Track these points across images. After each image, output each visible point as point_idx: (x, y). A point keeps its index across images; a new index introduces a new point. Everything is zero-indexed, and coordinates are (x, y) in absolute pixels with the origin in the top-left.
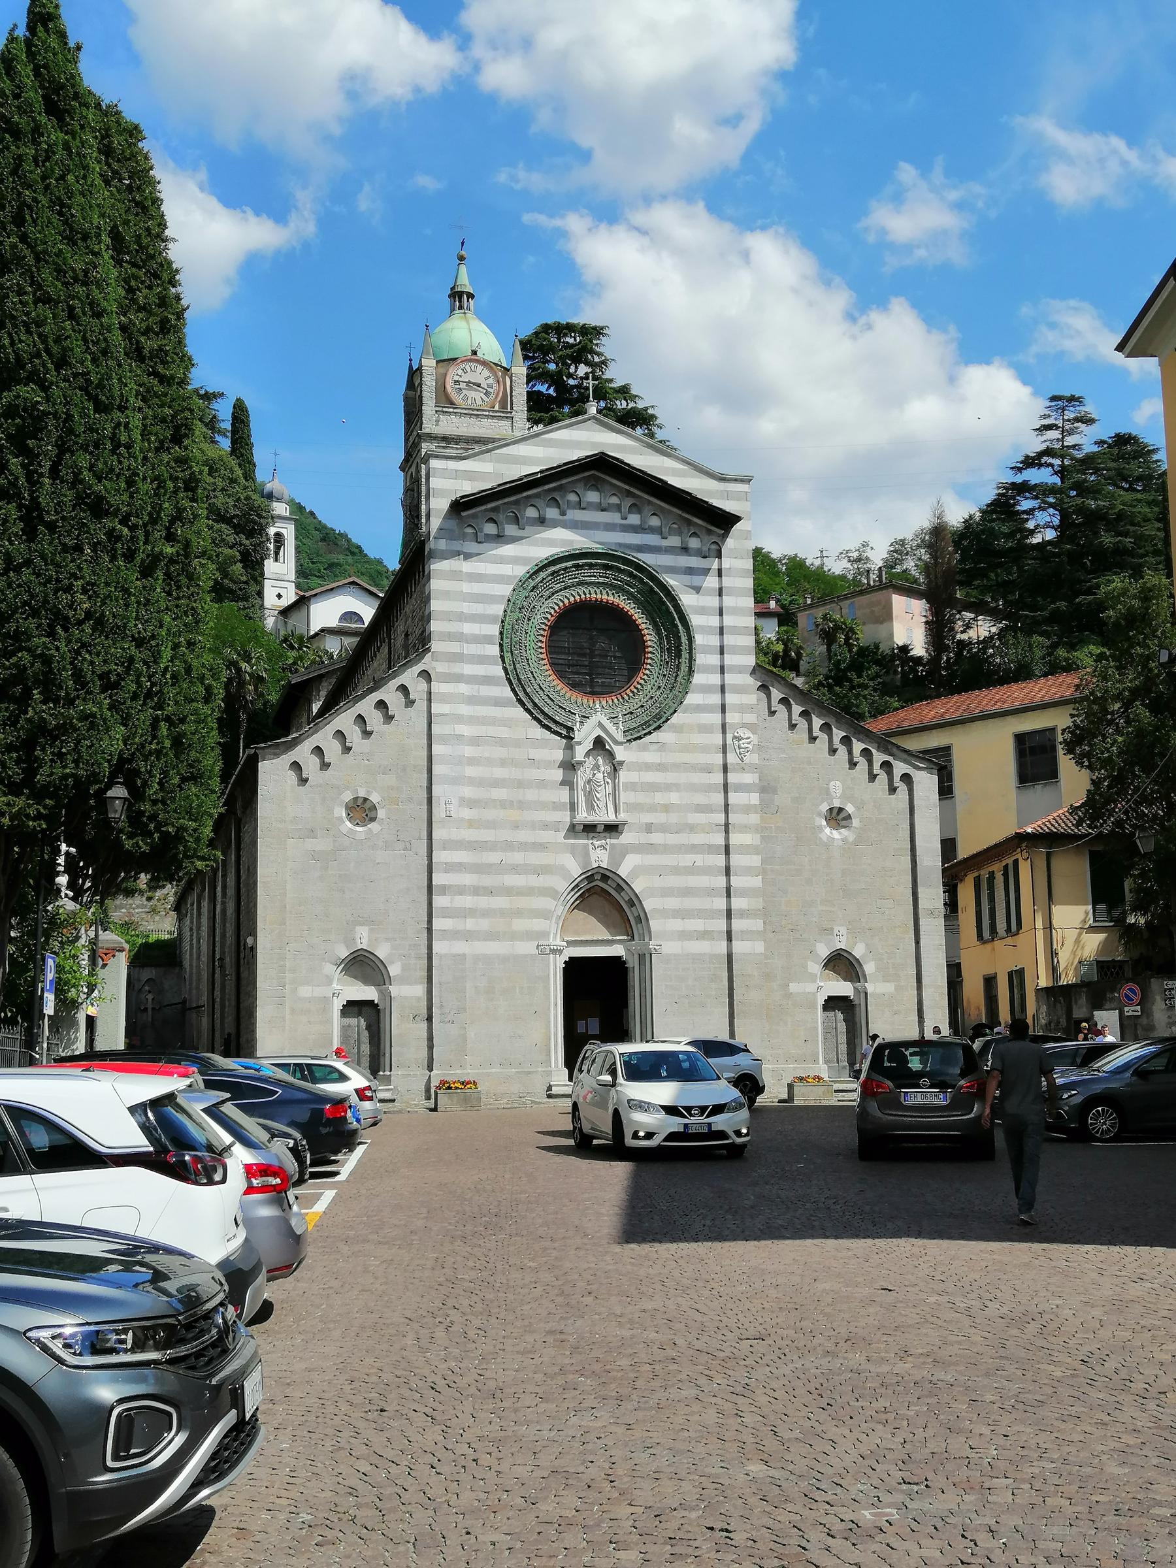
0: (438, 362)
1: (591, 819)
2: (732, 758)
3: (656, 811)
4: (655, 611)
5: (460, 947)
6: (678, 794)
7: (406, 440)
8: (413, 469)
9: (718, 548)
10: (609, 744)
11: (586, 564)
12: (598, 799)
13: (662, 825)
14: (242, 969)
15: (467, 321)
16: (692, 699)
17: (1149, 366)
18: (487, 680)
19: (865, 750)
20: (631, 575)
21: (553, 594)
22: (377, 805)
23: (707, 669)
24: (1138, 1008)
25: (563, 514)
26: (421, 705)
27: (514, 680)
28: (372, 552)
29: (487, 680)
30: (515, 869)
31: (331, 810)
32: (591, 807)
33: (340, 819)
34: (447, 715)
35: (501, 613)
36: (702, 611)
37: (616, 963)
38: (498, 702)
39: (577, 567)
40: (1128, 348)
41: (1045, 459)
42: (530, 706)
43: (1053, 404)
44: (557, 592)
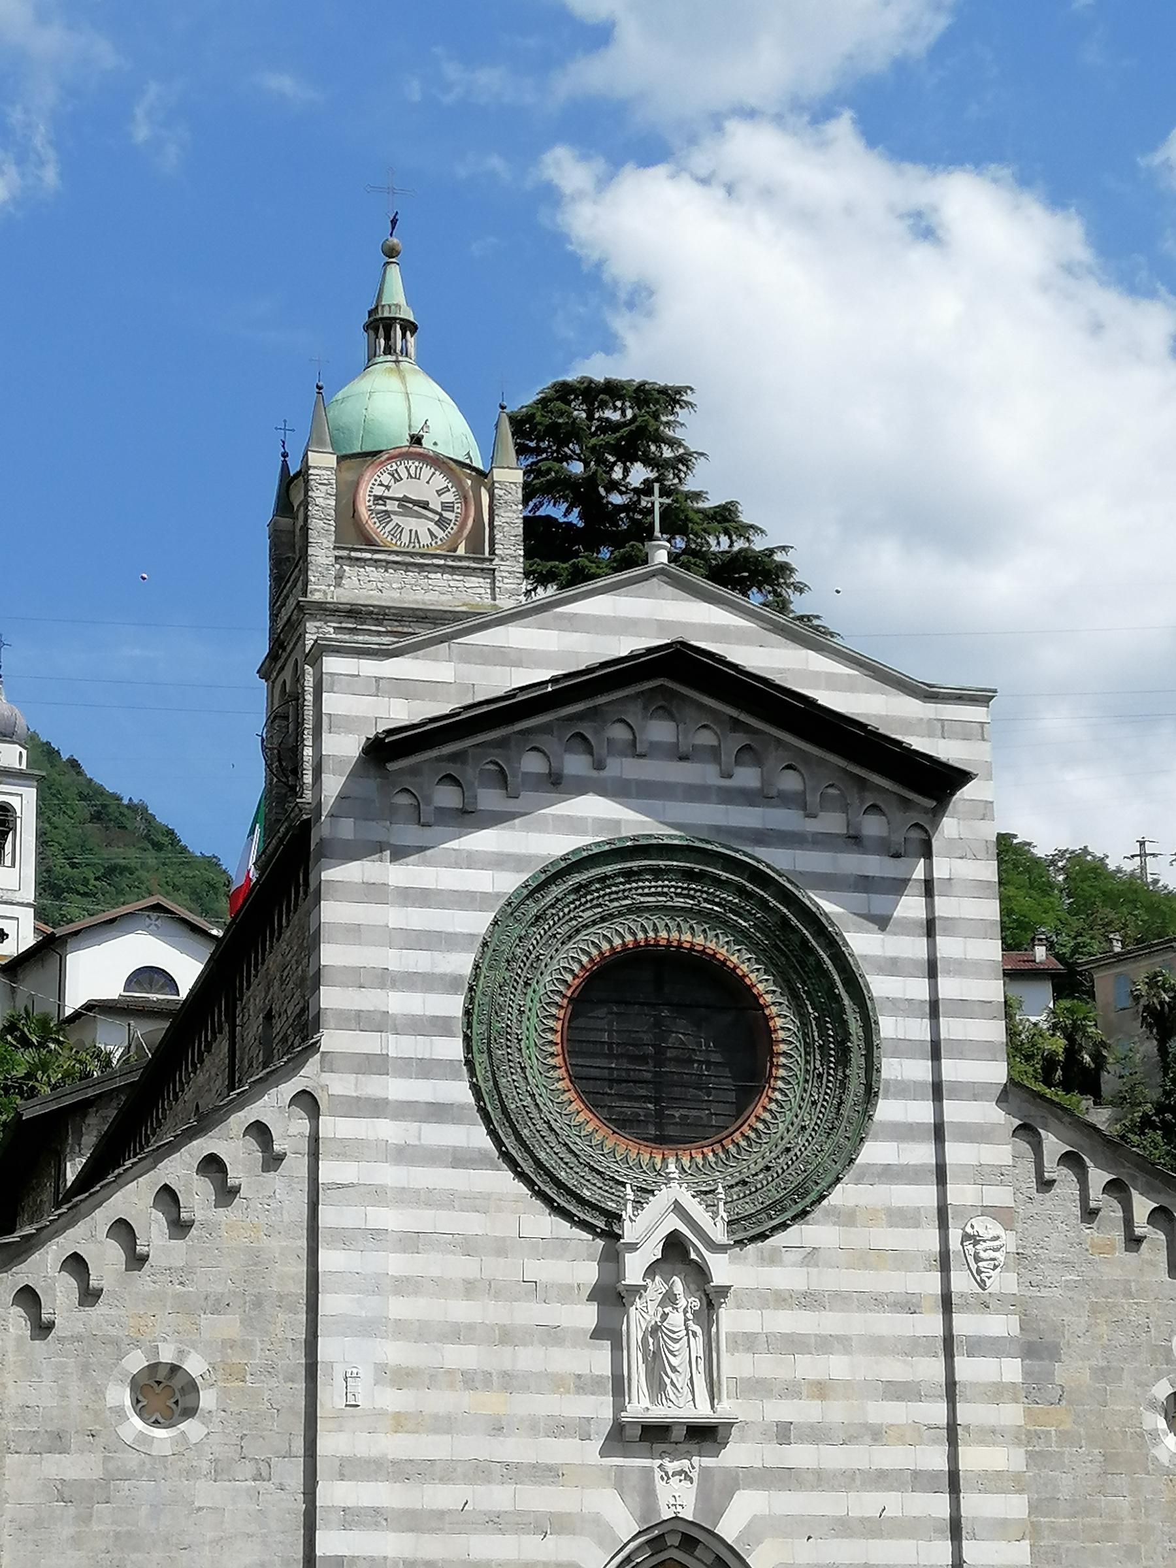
1: (660, 1412)
2: (961, 1282)
6: (846, 1358)
7: (274, 617)
8: (287, 674)
9: (924, 836)
12: (674, 1369)
13: (812, 1426)
15: (403, 379)
16: (873, 1152)
18: (438, 1112)
20: (741, 891)
22: (199, 1381)
23: (905, 1090)
25: (599, 766)
26: (296, 1165)
29: (438, 1112)
30: (496, 1522)
31: (99, 1392)
32: (657, 1387)
33: (119, 1412)
35: (468, 970)
36: (893, 966)
38: (460, 1159)
42: (528, 1167)
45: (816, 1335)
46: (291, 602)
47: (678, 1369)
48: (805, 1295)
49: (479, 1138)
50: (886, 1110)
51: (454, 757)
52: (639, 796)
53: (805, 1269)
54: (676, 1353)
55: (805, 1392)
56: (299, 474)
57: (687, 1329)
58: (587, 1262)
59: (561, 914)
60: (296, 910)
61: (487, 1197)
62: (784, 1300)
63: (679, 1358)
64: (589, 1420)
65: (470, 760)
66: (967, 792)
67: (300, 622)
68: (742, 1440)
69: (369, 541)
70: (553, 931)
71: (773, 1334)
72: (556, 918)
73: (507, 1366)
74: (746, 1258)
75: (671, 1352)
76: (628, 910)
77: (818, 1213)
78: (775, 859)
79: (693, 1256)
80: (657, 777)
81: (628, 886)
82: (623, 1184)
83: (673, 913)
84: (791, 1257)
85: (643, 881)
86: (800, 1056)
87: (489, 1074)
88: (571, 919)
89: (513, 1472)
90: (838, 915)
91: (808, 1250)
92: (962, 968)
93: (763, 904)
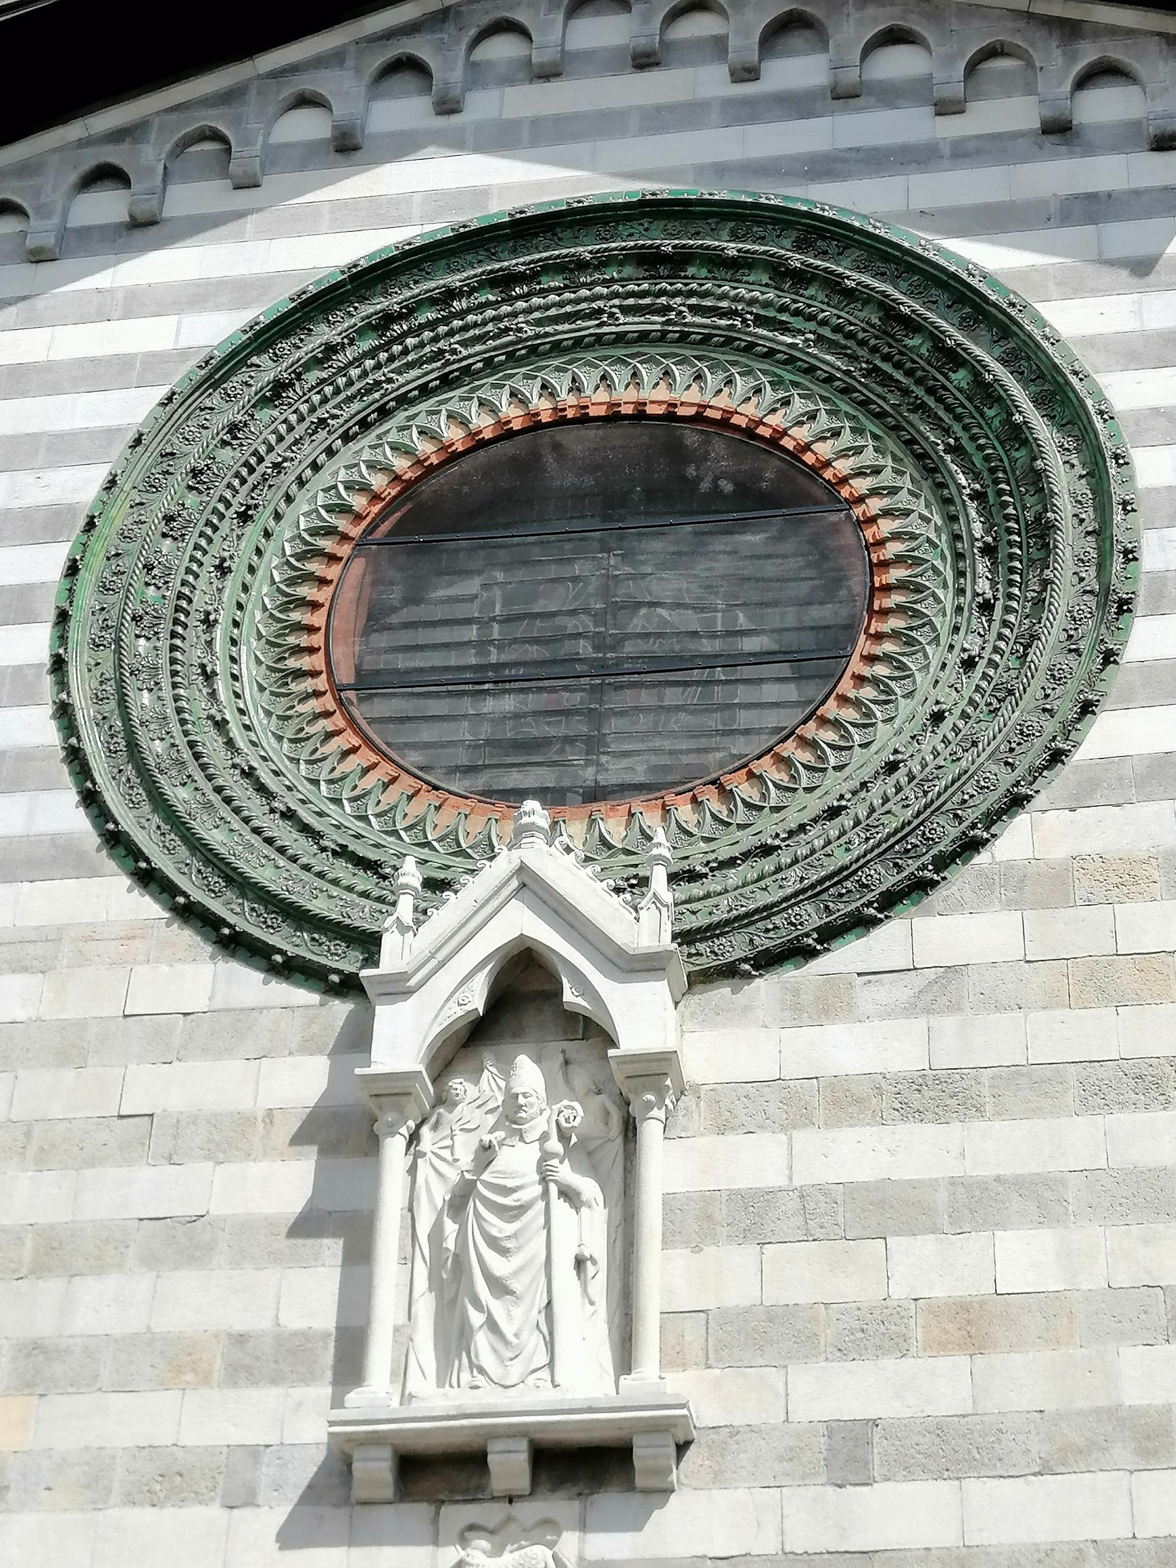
3: (899, 1346)
4: (919, 407)
5: (502, 1457)
6: (1046, 1237)
11: (549, 268)
12: (499, 1287)
13: (940, 1429)
21: (384, 413)
28: (993, 827)
39: (504, 282)
44: (404, 401)
45: (953, 1182)
47: (515, 1285)
48: (918, 1083)
51: (119, 135)
52: (534, 142)
53: (920, 1024)
54: (508, 1244)
55: (918, 1334)
57: (544, 1181)
58: (299, 1059)
59: (341, 381)
61: (52, 937)
62: (858, 1101)
63: (516, 1261)
64: (254, 1452)
65: (153, 137)
68: (720, 1479)
70: (321, 413)
71: (820, 1188)
72: (328, 390)
73: (44, 1327)
74: (746, 1009)
75: (494, 1243)
76: (510, 356)
77: (180, 375)
79: (569, 996)
81: (506, 309)
83: (619, 352)
84: (870, 996)
85: (544, 292)
86: (945, 586)
87: (110, 688)
88: (369, 391)
90: (1023, 274)
91: (931, 974)
93: (833, 285)
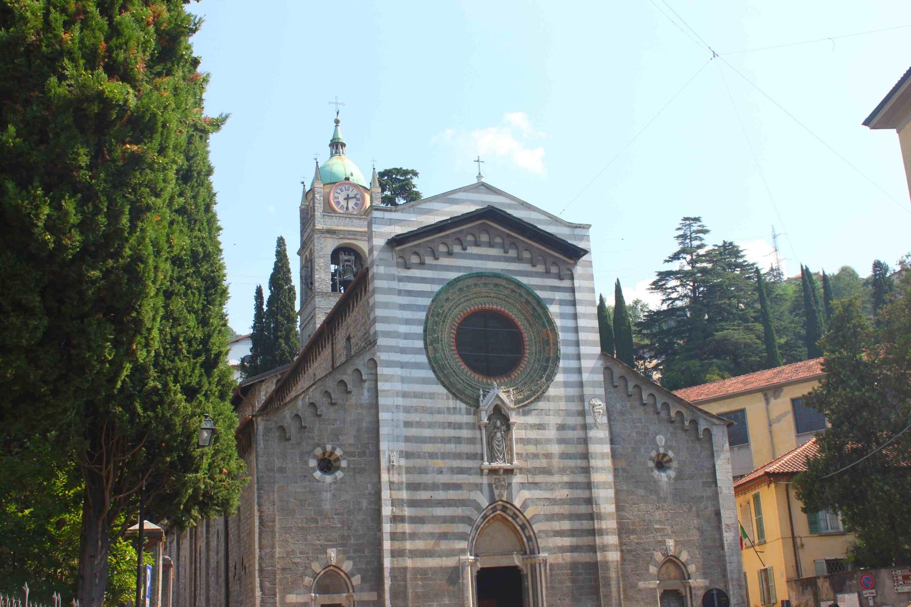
0: (324, 185)
7: (302, 236)
8: (307, 253)
9: (570, 273)
10: (504, 410)
14: (230, 585)
15: (342, 160)
17: (890, 136)
18: (417, 366)
19: (678, 412)
22: (340, 457)
24: (874, 591)
25: (465, 249)
27: (436, 365)
29: (417, 366)
30: (441, 503)
31: (306, 463)
34: (389, 391)
35: (424, 317)
37: (514, 571)
38: (424, 381)
40: (875, 121)
41: (682, 255)
43: (684, 222)
46: (309, 230)
48: (540, 425)
49: (430, 374)
50: (562, 364)
56: (311, 190)
60: (361, 300)
66: (585, 258)
67: (312, 236)
69: (334, 211)
78: (524, 280)
80: (484, 253)
82: (479, 390)
89: (447, 487)
92: (585, 316)
